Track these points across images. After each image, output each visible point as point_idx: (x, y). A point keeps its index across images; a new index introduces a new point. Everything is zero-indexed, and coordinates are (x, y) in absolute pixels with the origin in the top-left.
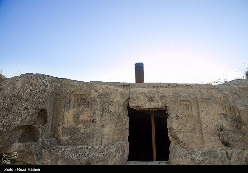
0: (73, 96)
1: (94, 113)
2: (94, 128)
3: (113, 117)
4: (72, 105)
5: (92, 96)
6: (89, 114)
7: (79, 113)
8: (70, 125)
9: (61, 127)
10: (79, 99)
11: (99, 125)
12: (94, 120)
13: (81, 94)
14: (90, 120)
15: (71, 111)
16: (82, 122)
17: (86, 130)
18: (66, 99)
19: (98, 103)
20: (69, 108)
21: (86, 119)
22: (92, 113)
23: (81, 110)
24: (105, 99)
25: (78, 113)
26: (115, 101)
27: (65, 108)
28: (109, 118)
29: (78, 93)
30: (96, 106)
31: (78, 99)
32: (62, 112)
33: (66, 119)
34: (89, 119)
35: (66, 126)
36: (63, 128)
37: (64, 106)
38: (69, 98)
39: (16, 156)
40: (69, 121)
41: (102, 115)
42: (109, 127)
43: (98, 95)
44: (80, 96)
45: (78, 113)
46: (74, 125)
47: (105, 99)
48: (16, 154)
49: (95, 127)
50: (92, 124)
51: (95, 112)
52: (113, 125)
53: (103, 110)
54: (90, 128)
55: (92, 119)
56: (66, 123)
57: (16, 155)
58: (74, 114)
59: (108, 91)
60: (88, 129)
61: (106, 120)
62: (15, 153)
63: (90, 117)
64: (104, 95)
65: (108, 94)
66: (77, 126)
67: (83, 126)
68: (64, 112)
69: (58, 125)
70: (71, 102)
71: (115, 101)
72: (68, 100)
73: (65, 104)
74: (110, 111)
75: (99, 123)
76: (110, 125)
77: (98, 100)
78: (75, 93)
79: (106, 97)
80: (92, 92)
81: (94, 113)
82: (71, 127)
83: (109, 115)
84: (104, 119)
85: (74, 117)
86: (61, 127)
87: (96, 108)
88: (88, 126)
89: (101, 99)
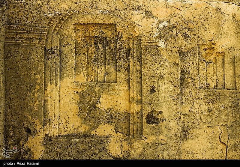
0: (69, 30)
1: (152, 91)
2: (158, 139)
3: (218, 105)
4: (71, 61)
5: (139, 31)
6: (134, 94)
7: (97, 89)
8: (70, 130)
9: (40, 137)
10: (93, 41)
11: (173, 132)
12: (155, 115)
13: (96, 25)
14: (140, 114)
15: (68, 82)
16: (110, 118)
17: (126, 147)
18: (47, 40)
19: (165, 57)
20: (61, 71)
21: (122, 110)
22: (146, 90)
23: (101, 77)
24: (182, 42)
25: (92, 89)
26: (219, 48)
27: (49, 72)
28: (204, 107)
29: (87, 19)
30: (157, 66)
31: (87, 39)
32: (38, 87)
33: (54, 110)
34: (135, 108)
35: (54, 132)
36: (48, 140)
37: (41, 66)
38: (56, 38)
39: (15, 151)
40: (63, 115)
41: (179, 98)
42: (204, 136)
43: (161, 27)
44: (92, 31)
45: (92, 89)
46: (83, 129)
47: (182, 42)
48: (15, 149)
49: (161, 137)
50: (147, 127)
51: (156, 85)
52: (218, 130)
53: (182, 79)
54: (143, 140)
55: (147, 110)
56: (56, 122)
57: (16, 150)
58: (80, 91)
59: (188, 15)
60: (135, 145)
61: (192, 112)
62: (15, 147)
63: (140, 102)
64: (178, 27)
65: (190, 26)
66: (93, 133)
67: (113, 133)
68: (45, 86)
69: (29, 131)
70: (66, 50)
71: (219, 48)
72: (55, 44)
73: (46, 58)
74: (203, 81)
75: (172, 124)
76: (210, 130)
77: (161, 44)
78: (76, 20)
79: (185, 36)
80: (136, 17)
81: (152, 91)
82: (74, 135)
83: (202, 96)
84: (186, 109)
85: (80, 103)
86: (40, 137)
87: (158, 72)
88: (133, 132)
89: (172, 40)
